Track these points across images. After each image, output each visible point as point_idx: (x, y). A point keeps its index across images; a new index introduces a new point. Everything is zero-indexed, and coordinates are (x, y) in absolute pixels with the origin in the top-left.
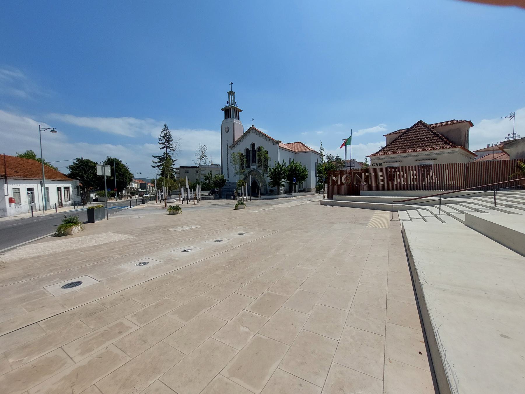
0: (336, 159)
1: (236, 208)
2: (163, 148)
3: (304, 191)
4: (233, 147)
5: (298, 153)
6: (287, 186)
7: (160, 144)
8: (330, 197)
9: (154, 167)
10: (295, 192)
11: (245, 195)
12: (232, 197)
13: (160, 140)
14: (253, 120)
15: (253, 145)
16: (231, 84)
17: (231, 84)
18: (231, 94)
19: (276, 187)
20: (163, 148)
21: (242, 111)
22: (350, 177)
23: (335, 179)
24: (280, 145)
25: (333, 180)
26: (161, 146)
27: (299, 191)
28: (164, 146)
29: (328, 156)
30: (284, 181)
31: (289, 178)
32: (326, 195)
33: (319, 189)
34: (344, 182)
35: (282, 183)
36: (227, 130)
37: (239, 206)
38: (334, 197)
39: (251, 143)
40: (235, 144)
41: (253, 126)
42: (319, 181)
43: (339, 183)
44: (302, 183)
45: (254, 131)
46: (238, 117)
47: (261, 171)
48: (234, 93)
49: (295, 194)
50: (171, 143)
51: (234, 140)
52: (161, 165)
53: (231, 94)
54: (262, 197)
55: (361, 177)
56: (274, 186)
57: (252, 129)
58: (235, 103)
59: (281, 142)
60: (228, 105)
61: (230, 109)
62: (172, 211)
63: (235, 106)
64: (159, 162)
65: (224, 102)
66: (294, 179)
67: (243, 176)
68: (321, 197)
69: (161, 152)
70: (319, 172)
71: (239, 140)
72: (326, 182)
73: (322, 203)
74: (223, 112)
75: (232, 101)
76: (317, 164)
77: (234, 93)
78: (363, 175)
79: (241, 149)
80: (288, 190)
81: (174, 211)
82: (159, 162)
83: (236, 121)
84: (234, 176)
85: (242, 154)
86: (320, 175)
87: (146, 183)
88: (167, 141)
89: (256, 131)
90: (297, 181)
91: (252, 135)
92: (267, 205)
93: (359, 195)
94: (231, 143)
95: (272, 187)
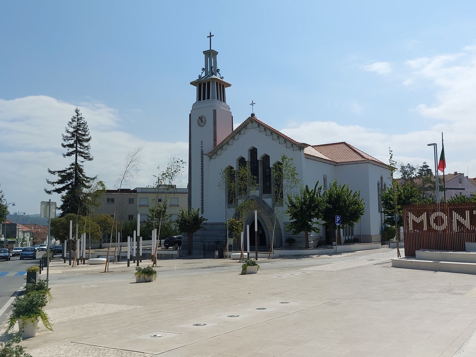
0: (421, 174)
1: (244, 273)
2: (69, 154)
3: (356, 240)
4: (213, 153)
5: (342, 164)
6: (322, 232)
7: (64, 146)
8: (410, 254)
9: (49, 192)
10: (339, 243)
11: (245, 250)
12: (217, 253)
13: (66, 138)
14: (253, 104)
15: (253, 152)
16: (210, 36)
17: (210, 36)
18: (210, 54)
19: (303, 233)
20: (69, 154)
21: (229, 85)
22: (445, 218)
23: (418, 220)
24: (307, 151)
25: (414, 222)
26: (66, 150)
27: (348, 242)
28: (71, 150)
29: (403, 167)
30: (317, 223)
31: (328, 216)
32: (402, 251)
33: (386, 237)
34: (434, 226)
35: (314, 226)
36: (202, 120)
37: (249, 268)
38: (418, 253)
39: (250, 147)
40: (217, 149)
41: (253, 115)
42: (386, 221)
43: (425, 228)
44: (352, 225)
45: (255, 125)
46: (222, 97)
47: (269, 201)
48: (215, 53)
49: (339, 248)
50: (85, 144)
51: (215, 140)
52: (63, 189)
53: (210, 54)
54: (277, 252)
55: (464, 218)
56: (299, 230)
57: (252, 119)
58: (218, 70)
59: (307, 145)
60: (204, 75)
61: (209, 83)
62: (142, 276)
63: (218, 77)
64: (60, 182)
65: (197, 70)
66: (338, 218)
67: (232, 211)
68: (391, 254)
69: (65, 163)
70: (386, 203)
71: (226, 142)
72: (400, 223)
73: (396, 265)
74: (195, 89)
75: (211, 69)
76: (381, 186)
77: (215, 53)
78: (467, 213)
79: (229, 158)
80: (324, 239)
81: (146, 276)
82: (60, 182)
83: (218, 104)
84: (216, 210)
85: (231, 168)
86: (389, 211)
87: (15, 225)
88: (79, 141)
89: (260, 124)
90: (343, 221)
91: (252, 132)
92: (282, 269)
93: (464, 250)
94: (209, 147)
95: (295, 233)
